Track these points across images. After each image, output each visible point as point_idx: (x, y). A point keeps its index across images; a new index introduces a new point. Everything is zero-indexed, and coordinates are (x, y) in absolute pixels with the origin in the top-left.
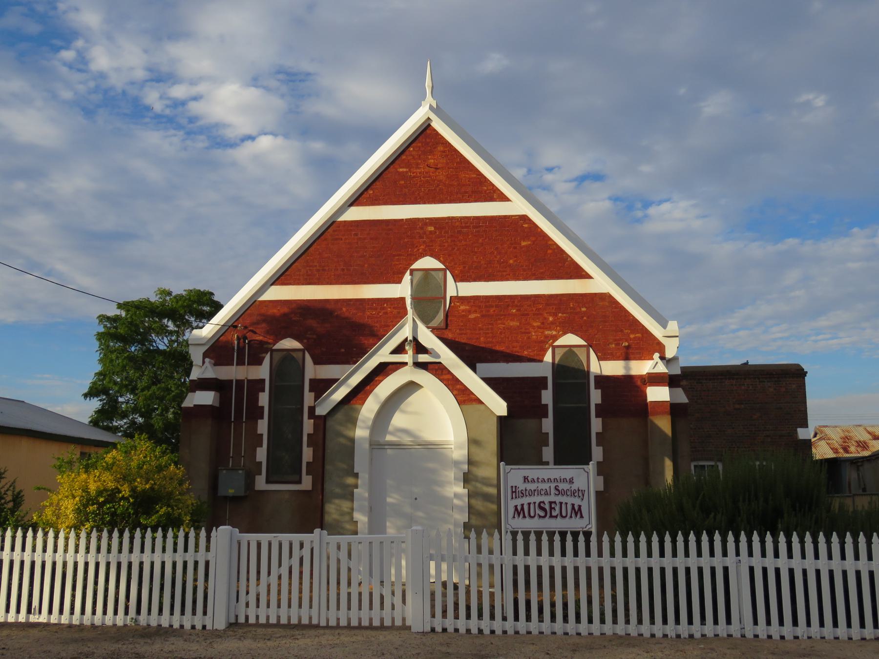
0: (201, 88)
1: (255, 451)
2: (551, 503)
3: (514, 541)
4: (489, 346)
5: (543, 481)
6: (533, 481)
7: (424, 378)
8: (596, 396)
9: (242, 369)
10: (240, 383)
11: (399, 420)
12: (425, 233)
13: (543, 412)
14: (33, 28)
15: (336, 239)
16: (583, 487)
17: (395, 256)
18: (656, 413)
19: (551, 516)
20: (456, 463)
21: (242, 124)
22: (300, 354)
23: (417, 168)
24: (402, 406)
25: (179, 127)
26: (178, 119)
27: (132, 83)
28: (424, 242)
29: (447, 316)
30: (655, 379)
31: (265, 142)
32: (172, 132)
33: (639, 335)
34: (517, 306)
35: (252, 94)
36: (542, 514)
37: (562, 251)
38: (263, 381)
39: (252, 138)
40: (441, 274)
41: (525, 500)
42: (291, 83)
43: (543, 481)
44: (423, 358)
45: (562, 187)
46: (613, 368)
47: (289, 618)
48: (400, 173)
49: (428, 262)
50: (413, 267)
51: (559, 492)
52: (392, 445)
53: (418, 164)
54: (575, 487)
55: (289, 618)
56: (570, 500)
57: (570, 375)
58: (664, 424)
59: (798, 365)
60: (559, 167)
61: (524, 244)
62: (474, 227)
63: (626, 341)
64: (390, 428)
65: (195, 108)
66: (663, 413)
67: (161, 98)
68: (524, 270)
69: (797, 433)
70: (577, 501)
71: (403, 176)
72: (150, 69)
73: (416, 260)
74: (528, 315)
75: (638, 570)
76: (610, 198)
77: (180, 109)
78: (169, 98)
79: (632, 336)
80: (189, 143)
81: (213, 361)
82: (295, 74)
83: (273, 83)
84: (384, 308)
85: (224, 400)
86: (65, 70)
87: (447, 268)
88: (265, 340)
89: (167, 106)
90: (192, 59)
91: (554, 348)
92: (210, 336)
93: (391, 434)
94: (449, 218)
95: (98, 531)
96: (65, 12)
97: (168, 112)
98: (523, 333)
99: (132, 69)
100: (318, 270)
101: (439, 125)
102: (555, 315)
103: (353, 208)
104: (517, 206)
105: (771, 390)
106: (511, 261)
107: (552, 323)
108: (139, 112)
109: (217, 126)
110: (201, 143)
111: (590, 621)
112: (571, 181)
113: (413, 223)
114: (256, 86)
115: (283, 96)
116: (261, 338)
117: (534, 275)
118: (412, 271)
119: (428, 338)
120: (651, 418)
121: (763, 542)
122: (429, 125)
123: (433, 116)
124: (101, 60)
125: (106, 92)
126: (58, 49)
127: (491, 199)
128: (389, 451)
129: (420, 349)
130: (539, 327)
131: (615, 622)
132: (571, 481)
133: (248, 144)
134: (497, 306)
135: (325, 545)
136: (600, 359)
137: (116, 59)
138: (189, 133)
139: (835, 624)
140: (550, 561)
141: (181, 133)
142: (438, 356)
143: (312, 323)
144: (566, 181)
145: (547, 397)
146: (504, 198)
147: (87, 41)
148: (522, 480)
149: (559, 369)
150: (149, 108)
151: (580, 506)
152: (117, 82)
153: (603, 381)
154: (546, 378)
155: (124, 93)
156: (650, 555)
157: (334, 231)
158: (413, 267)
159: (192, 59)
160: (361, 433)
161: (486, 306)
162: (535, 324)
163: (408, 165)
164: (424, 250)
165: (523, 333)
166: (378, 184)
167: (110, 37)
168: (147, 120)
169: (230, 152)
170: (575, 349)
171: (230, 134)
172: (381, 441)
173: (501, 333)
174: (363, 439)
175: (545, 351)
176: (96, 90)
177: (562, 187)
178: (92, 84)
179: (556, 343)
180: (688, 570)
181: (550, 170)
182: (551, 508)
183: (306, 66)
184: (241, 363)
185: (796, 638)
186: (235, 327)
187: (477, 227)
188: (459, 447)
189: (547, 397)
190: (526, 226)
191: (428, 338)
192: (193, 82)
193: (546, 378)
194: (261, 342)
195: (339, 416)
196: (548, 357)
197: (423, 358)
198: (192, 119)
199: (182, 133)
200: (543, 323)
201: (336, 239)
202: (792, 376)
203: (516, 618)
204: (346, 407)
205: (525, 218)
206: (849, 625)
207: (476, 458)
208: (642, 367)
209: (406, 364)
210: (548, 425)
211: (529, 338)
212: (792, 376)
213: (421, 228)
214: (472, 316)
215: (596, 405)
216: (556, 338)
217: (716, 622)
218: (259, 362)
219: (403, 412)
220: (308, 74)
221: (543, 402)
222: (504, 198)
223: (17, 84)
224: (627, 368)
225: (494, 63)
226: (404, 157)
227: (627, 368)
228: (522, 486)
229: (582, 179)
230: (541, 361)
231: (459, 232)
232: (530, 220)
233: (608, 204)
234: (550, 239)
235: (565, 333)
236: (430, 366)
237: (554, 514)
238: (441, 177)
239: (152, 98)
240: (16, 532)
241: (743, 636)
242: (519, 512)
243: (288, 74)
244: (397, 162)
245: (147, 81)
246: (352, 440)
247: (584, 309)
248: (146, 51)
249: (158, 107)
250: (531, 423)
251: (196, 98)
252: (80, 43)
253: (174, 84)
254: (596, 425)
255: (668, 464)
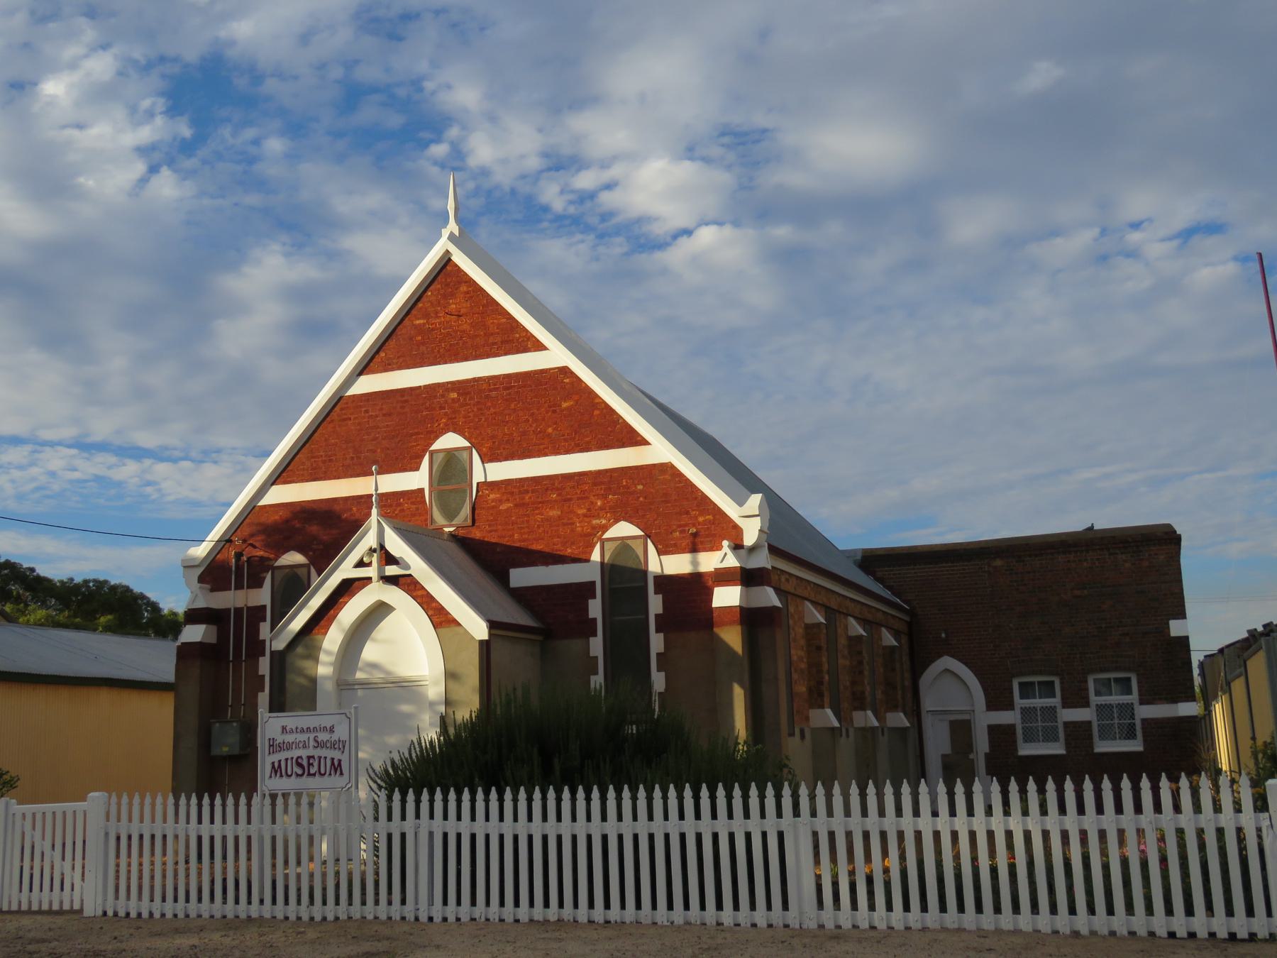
0: (615, 172)
1: (256, 697)
2: (309, 758)
3: (273, 805)
4: (523, 545)
5: (302, 731)
6: (292, 731)
7: (395, 596)
8: (655, 604)
9: (241, 593)
10: (238, 611)
11: (370, 652)
12: (446, 402)
13: (588, 628)
14: (395, 120)
15: (345, 420)
16: (345, 737)
17: (412, 435)
18: (723, 624)
19: (309, 774)
20: (432, 704)
21: (672, 214)
22: (305, 570)
23: (437, 317)
24: (374, 634)
25: (588, 229)
26: (590, 220)
27: (523, 177)
28: (446, 414)
29: (473, 509)
30: (724, 577)
31: (707, 236)
32: (579, 237)
33: (710, 517)
34: (557, 489)
35: (686, 170)
36: (300, 772)
37: (612, 411)
38: (264, 607)
39: (688, 232)
40: (465, 455)
41: (282, 756)
42: (739, 148)
43: (302, 731)
44: (391, 570)
45: (1156, 250)
46: (677, 564)
47: (51, 903)
48: (416, 327)
49: (451, 441)
50: (433, 448)
51: (319, 745)
52: (364, 684)
53: (437, 313)
54: (335, 737)
55: (51, 903)
56: (330, 754)
57: (624, 580)
58: (732, 637)
59: (1169, 526)
60: (1150, 220)
61: (565, 405)
62: (506, 388)
63: (694, 525)
64: (360, 664)
65: (608, 199)
66: (731, 623)
67: (562, 192)
68: (565, 440)
69: (1168, 628)
70: (336, 755)
71: (419, 329)
72: (545, 155)
73: (437, 437)
74: (570, 500)
75: (683, 837)
76: (1236, 259)
77: (588, 204)
78: (573, 191)
79: (701, 519)
80: (601, 249)
81: (208, 586)
82: (745, 134)
83: (716, 151)
84: (400, 505)
85: (223, 634)
86: (435, 170)
87: (473, 445)
88: (266, 555)
89: (571, 202)
90: (601, 132)
91: (603, 542)
92: (204, 554)
93: (361, 670)
94: (474, 380)
95: (1189, 775)
96: (433, 93)
97: (572, 210)
98: (564, 524)
99: (523, 157)
100: (324, 462)
101: (460, 259)
102: (604, 497)
103: (362, 378)
104: (555, 355)
105: (1128, 565)
106: (550, 430)
107: (601, 509)
108: (532, 215)
109: (641, 220)
110: (618, 246)
111: (1072, 911)
112: (1170, 239)
113: (432, 389)
114: (691, 159)
115: (729, 167)
116: (262, 553)
117: (578, 445)
118: (432, 453)
119: (396, 545)
120: (716, 630)
121: (1156, 790)
122: (450, 260)
123: (453, 249)
124: (482, 151)
125: (489, 193)
126: (425, 145)
127: (525, 350)
128: (360, 693)
129: (390, 559)
130: (585, 516)
131: (473, 903)
132: (332, 730)
133: (683, 240)
134: (533, 491)
135: (10, 817)
136: (660, 553)
137: (502, 146)
138: (601, 236)
139: (719, 907)
140: (915, 824)
141: (591, 237)
142: (408, 567)
143: (314, 529)
144: (1163, 240)
145: (595, 609)
146: (540, 347)
147: (464, 128)
148: (280, 730)
149: (610, 571)
150: (546, 209)
151: (340, 761)
152: (503, 178)
153: (665, 583)
154: (593, 583)
155: (513, 192)
156: (865, 813)
157: (342, 409)
158: (433, 448)
159: (601, 132)
160: (324, 669)
161: (520, 492)
162: (580, 512)
163: (426, 316)
164: (446, 425)
165: (564, 524)
166: (392, 343)
167: (492, 119)
168: (545, 224)
169: (659, 256)
170: (629, 542)
171: (658, 230)
172: (350, 679)
173: (539, 527)
174: (325, 678)
175: (593, 547)
176: (476, 192)
177: (1156, 250)
178: (471, 185)
179: (606, 535)
180: (699, 837)
181: (1136, 226)
182: (310, 765)
183: (760, 119)
184: (239, 586)
185: (473, 919)
186: (229, 541)
187: (507, 388)
188: (436, 683)
189: (595, 609)
190: (567, 381)
191: (396, 545)
192: (605, 164)
193: (593, 583)
194: (261, 557)
195: (300, 650)
196: (596, 556)
197: (391, 570)
198: (606, 216)
199: (592, 237)
200: (589, 510)
201: (345, 420)
202: (1163, 541)
203: (274, 902)
204: (307, 638)
205: (565, 371)
206: (576, 906)
207: (454, 697)
208: (710, 561)
209: (369, 579)
210: (596, 646)
211: (573, 531)
212: (1163, 541)
213: (443, 396)
214: (503, 507)
215: (657, 616)
216: (605, 528)
217: (670, 906)
218: (258, 583)
219: (374, 640)
220: (765, 131)
221: (591, 616)
222: (540, 347)
223: (375, 199)
224: (695, 563)
225: (1042, 75)
226: (420, 305)
227: (695, 563)
228: (280, 738)
229: (1187, 234)
230: (588, 560)
231: (487, 397)
232: (572, 373)
233: (1231, 268)
234: (597, 396)
235: (617, 521)
236: (402, 581)
237: (312, 771)
238: (465, 327)
239: (552, 194)
240: (517, 792)
241: (417, 919)
242: (276, 770)
243: (736, 135)
244: (413, 312)
245: (542, 171)
246: (313, 681)
247: (640, 487)
248: (540, 130)
249: (558, 205)
250: (575, 645)
251: (609, 186)
252: (454, 132)
253: (579, 170)
254: (657, 642)
255: (739, 694)
